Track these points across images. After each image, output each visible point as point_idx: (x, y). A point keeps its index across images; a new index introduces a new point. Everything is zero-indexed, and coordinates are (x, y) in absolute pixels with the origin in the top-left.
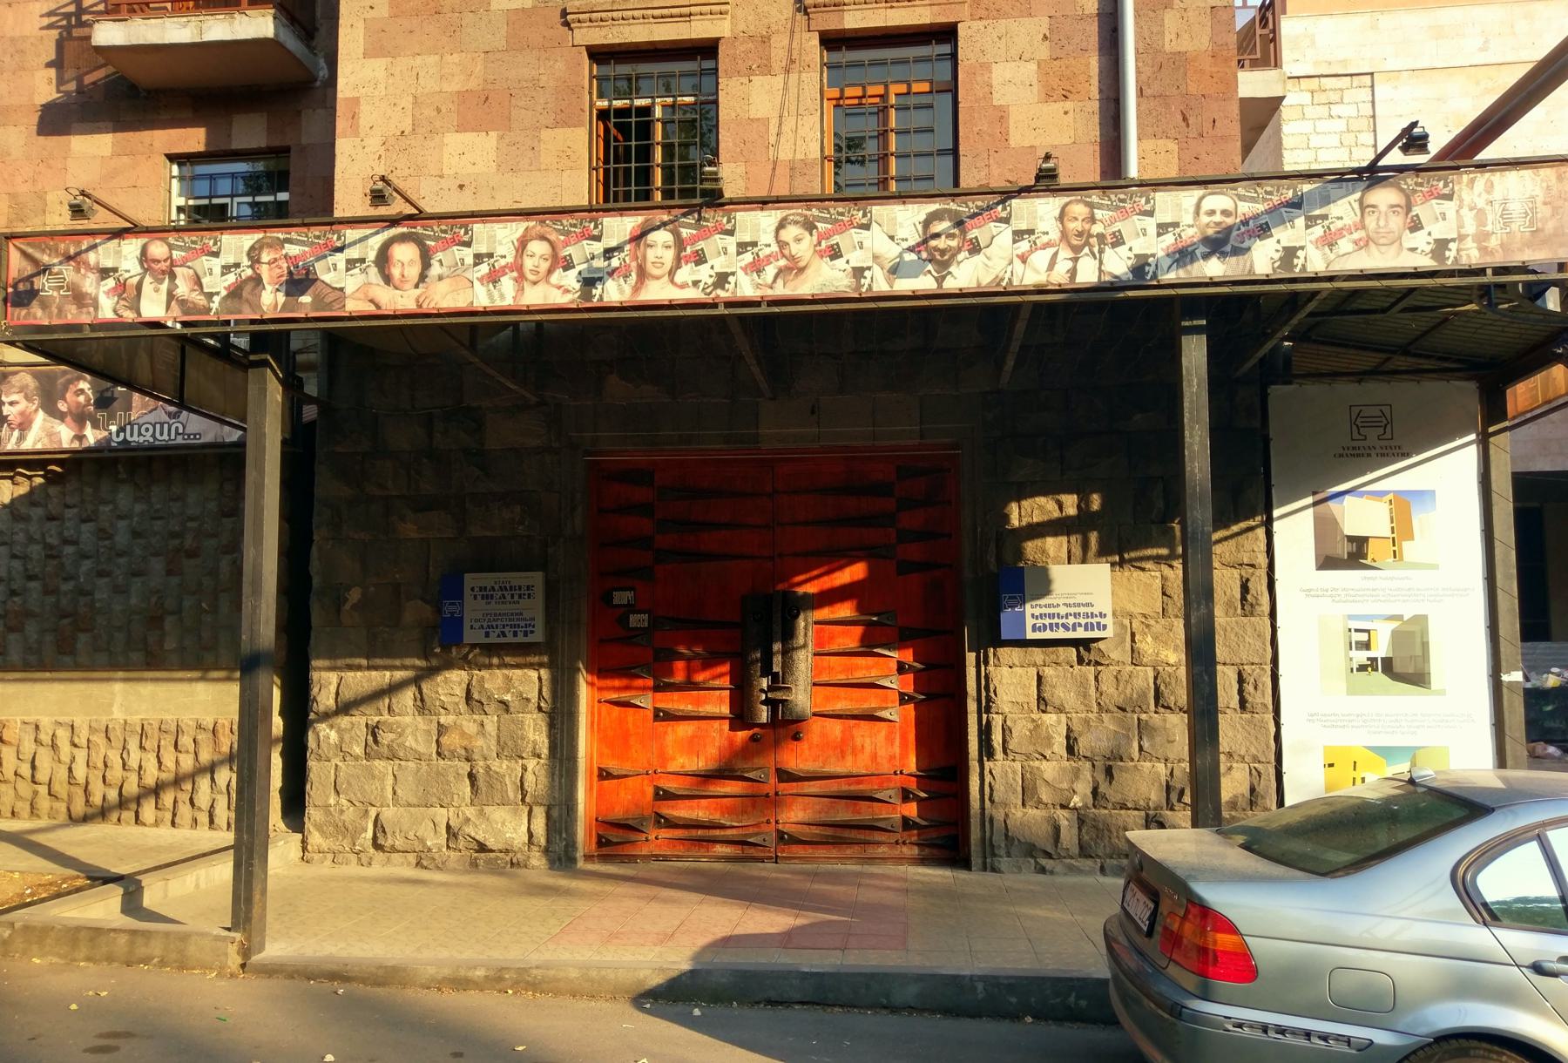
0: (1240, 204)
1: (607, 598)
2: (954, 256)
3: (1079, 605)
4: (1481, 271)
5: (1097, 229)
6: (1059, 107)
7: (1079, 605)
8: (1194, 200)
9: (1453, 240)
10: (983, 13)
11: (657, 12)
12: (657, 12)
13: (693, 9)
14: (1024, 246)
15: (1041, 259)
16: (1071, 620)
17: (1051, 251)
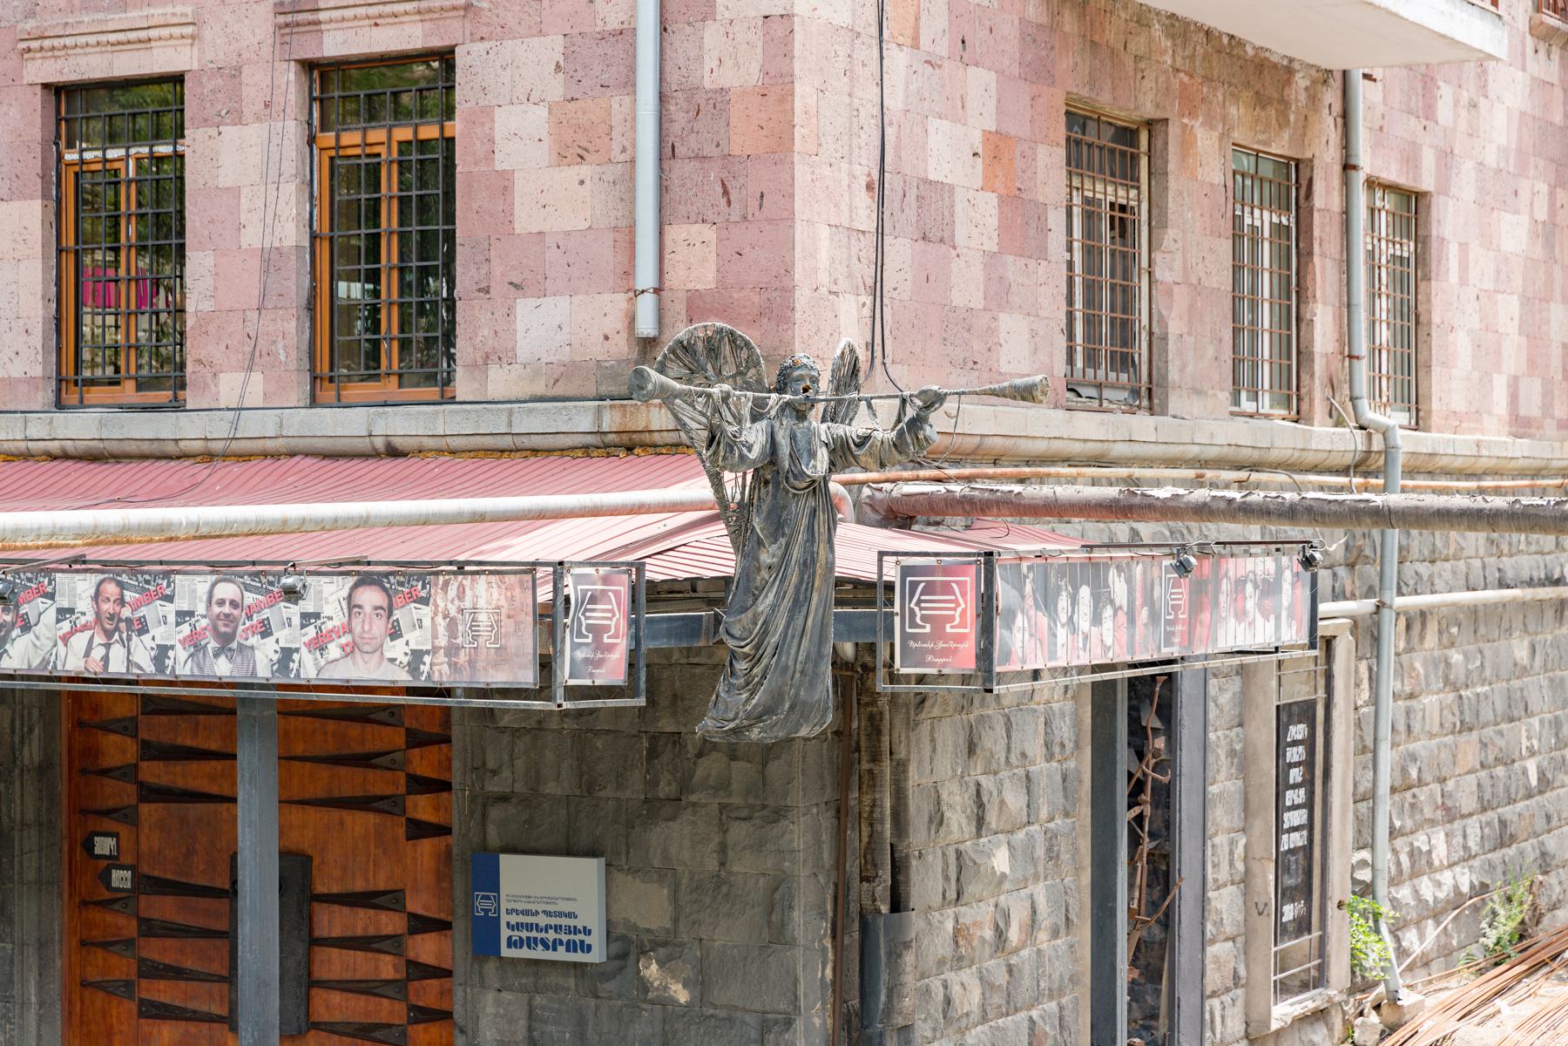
0: (246, 594)
1: (89, 846)
2: (9, 632)
3: (560, 914)
4: (447, 692)
5: (126, 612)
6: (573, 172)
7: (560, 914)
8: (207, 587)
9: (427, 652)
10: (484, 31)
11: (113, 38)
12: (113, 38)
13: (153, 33)
14: (66, 626)
15: (79, 641)
16: (551, 935)
17: (88, 634)
